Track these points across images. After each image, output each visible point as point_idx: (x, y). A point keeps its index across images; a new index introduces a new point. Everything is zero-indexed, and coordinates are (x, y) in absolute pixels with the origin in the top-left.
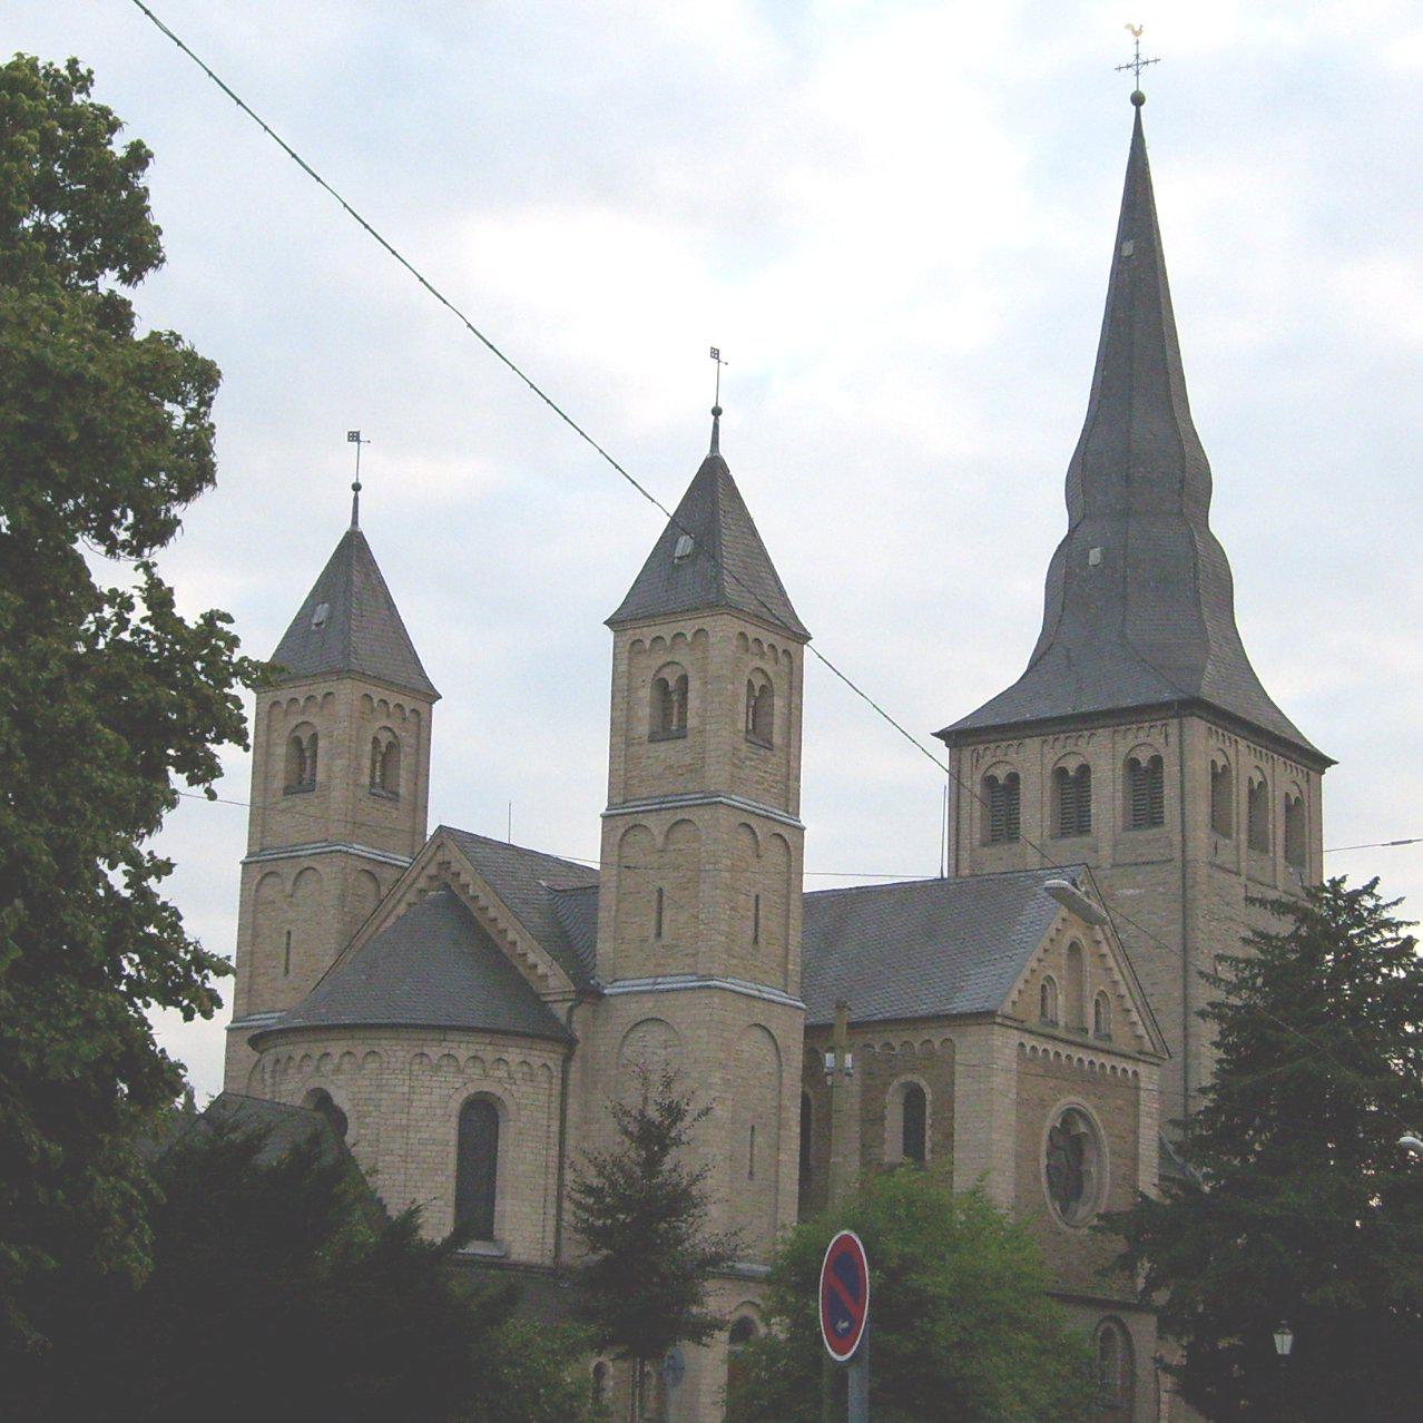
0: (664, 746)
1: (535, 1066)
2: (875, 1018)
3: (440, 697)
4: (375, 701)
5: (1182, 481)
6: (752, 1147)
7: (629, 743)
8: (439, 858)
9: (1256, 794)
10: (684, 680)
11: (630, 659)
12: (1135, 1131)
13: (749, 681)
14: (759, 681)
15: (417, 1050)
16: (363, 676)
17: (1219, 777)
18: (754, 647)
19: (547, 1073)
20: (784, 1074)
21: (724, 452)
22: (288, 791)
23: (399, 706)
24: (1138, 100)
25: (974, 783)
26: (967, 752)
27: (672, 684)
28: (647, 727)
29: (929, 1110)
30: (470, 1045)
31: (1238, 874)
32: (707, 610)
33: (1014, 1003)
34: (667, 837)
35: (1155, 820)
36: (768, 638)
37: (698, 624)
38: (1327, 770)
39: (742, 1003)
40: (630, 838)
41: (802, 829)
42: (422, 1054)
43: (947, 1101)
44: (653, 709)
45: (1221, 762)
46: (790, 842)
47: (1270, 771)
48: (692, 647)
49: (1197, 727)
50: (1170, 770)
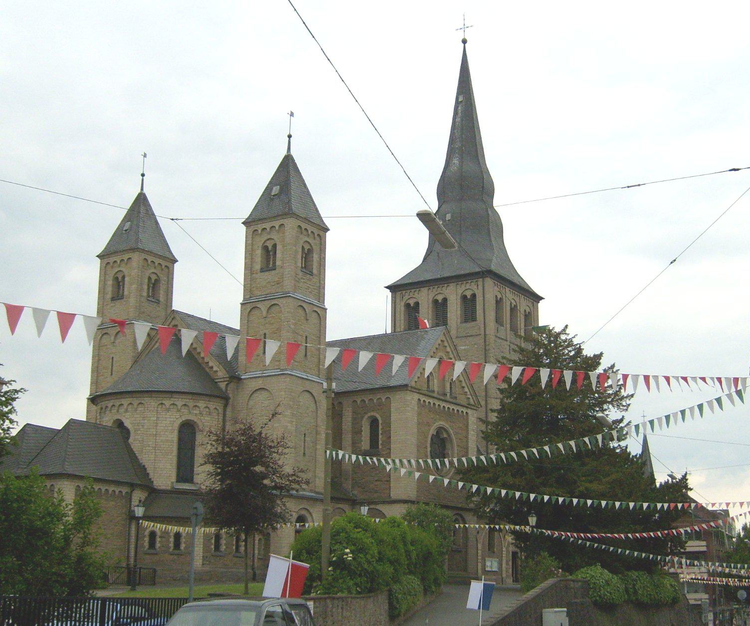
0: (267, 273)
1: (211, 409)
2: (358, 389)
3: (177, 261)
4: (149, 261)
5: (483, 187)
6: (304, 442)
7: (252, 274)
8: (173, 323)
9: (513, 310)
10: (275, 246)
11: (252, 237)
12: (467, 437)
13: (303, 246)
14: (307, 247)
15: (161, 402)
16: (143, 251)
17: (499, 302)
18: (305, 232)
19: (217, 412)
20: (318, 412)
21: (293, 153)
22: (113, 299)
23: (159, 264)
24: (464, 42)
25: (401, 308)
26: (398, 294)
27: (270, 248)
28: (260, 266)
29: (380, 427)
30: (183, 400)
31: (507, 341)
32: (286, 225)
33: (416, 382)
34: (268, 312)
35: (474, 319)
36: (310, 229)
37: (282, 222)
38: (540, 301)
39: (300, 381)
40: (252, 313)
41: (326, 309)
42: (162, 404)
43: (388, 424)
44: (263, 258)
45: (499, 297)
46: (321, 314)
47: (518, 301)
48: (278, 231)
49: (489, 282)
50: (479, 299)
